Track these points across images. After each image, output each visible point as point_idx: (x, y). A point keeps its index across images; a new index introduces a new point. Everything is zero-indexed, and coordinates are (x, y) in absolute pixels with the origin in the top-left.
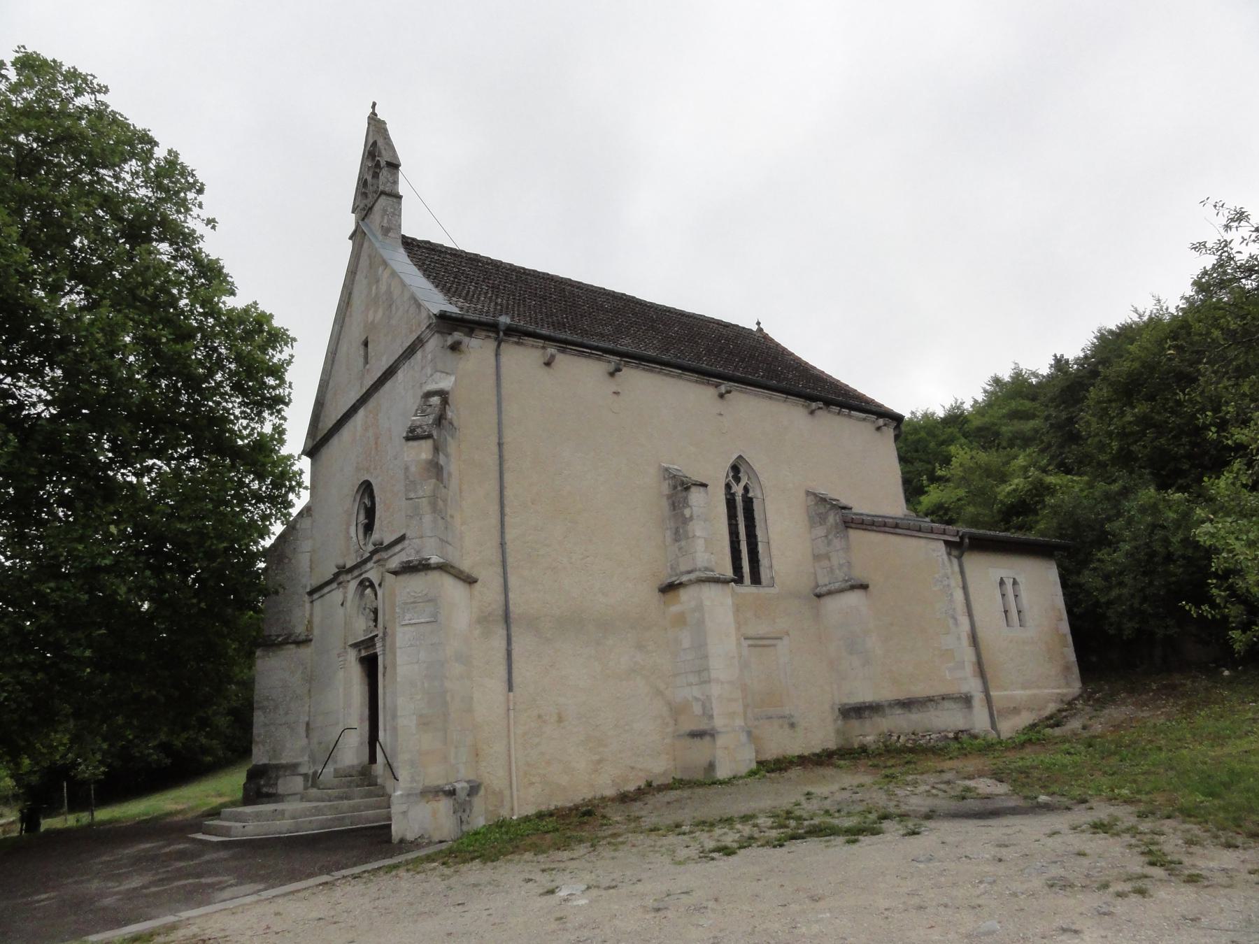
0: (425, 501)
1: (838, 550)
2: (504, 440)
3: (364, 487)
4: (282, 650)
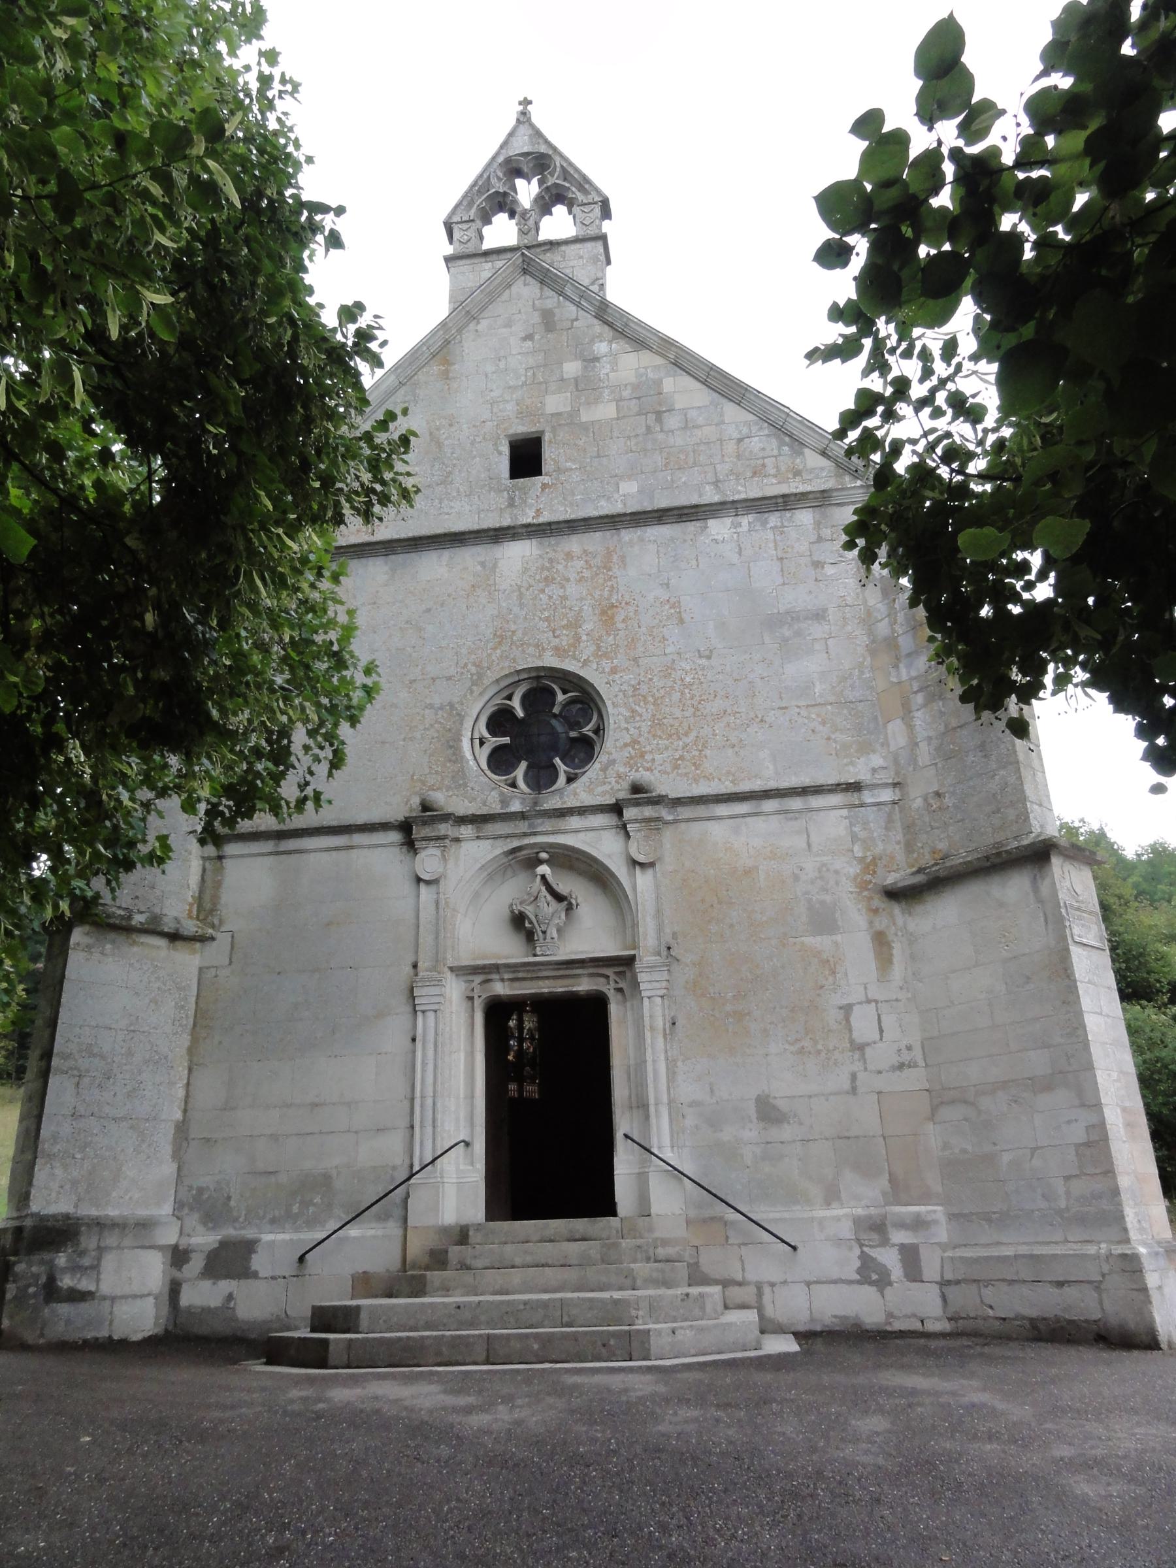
3: (533, 674)
4: (134, 943)
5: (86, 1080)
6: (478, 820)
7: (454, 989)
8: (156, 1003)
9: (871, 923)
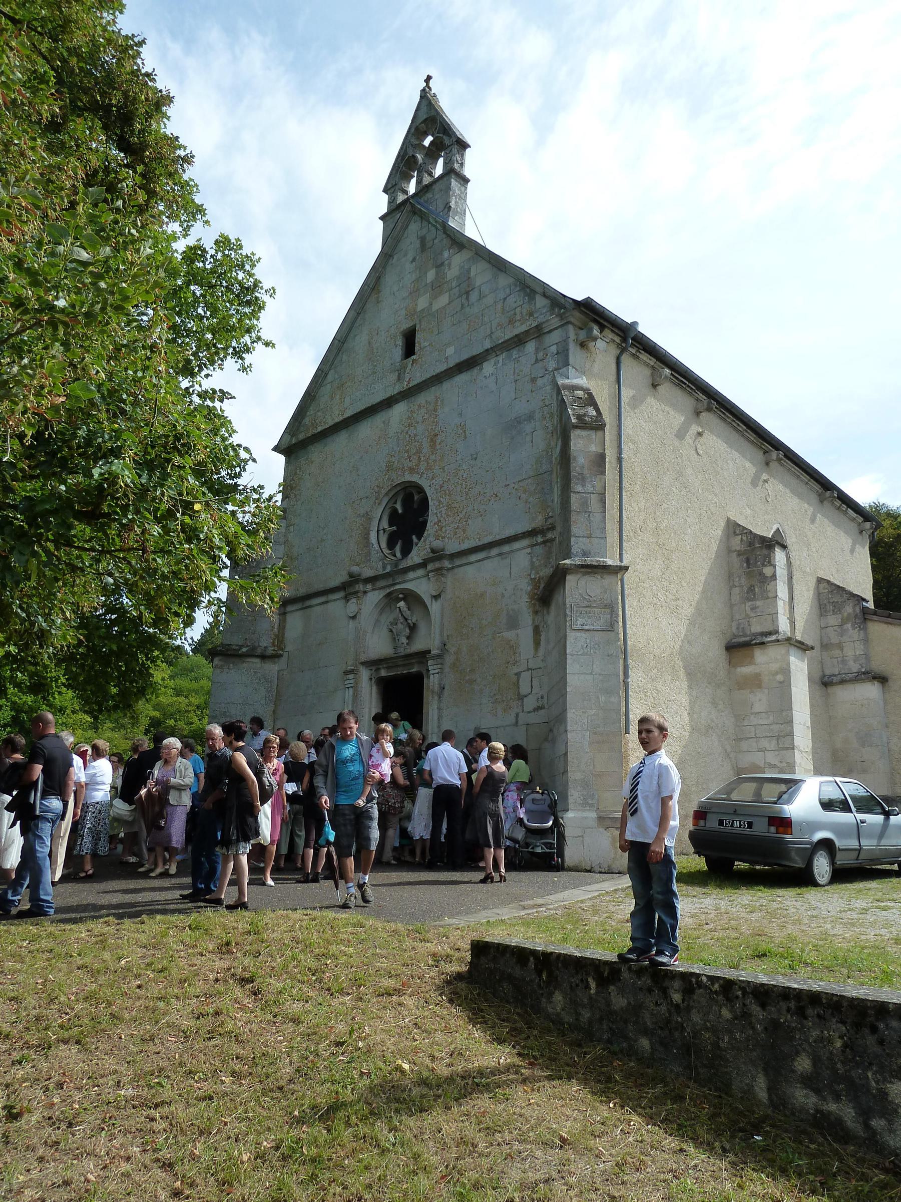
2: (623, 456)
4: (244, 662)
6: (372, 580)
7: (365, 674)
9: (534, 620)
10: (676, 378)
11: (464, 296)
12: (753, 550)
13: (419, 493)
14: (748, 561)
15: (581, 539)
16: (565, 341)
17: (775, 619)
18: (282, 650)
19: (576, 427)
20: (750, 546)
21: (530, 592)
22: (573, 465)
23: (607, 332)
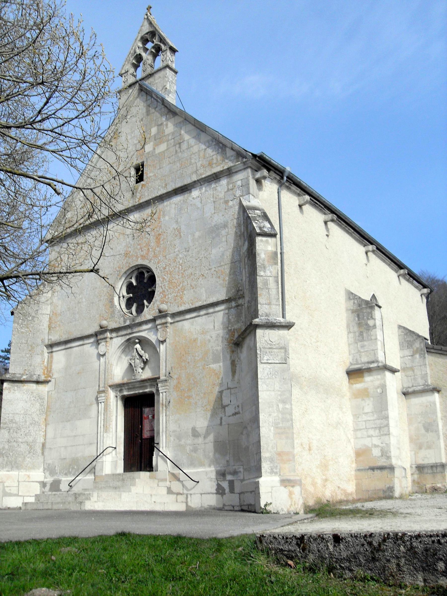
0: (271, 280)
1: (421, 366)
5: (12, 431)
7: (112, 394)
8: (33, 405)
9: (231, 357)
10: (313, 201)
11: (178, 146)
12: (361, 309)
13: (148, 272)
14: (358, 316)
15: (264, 305)
16: (247, 178)
17: (376, 353)
18: (50, 377)
19: (259, 235)
20: (359, 307)
21: (228, 339)
22: (258, 259)
23: (272, 173)
